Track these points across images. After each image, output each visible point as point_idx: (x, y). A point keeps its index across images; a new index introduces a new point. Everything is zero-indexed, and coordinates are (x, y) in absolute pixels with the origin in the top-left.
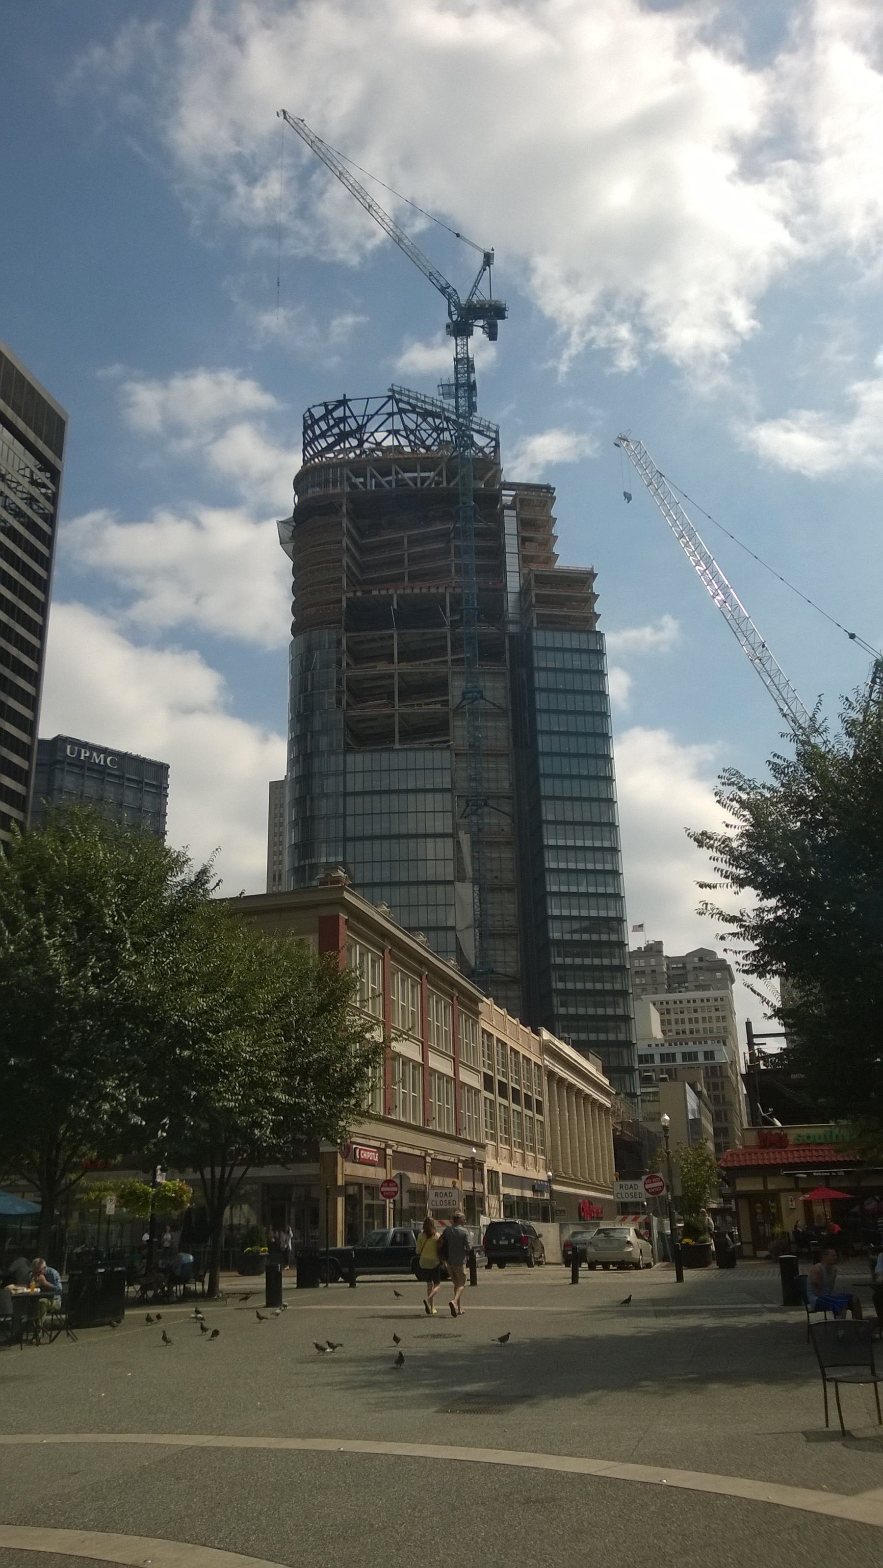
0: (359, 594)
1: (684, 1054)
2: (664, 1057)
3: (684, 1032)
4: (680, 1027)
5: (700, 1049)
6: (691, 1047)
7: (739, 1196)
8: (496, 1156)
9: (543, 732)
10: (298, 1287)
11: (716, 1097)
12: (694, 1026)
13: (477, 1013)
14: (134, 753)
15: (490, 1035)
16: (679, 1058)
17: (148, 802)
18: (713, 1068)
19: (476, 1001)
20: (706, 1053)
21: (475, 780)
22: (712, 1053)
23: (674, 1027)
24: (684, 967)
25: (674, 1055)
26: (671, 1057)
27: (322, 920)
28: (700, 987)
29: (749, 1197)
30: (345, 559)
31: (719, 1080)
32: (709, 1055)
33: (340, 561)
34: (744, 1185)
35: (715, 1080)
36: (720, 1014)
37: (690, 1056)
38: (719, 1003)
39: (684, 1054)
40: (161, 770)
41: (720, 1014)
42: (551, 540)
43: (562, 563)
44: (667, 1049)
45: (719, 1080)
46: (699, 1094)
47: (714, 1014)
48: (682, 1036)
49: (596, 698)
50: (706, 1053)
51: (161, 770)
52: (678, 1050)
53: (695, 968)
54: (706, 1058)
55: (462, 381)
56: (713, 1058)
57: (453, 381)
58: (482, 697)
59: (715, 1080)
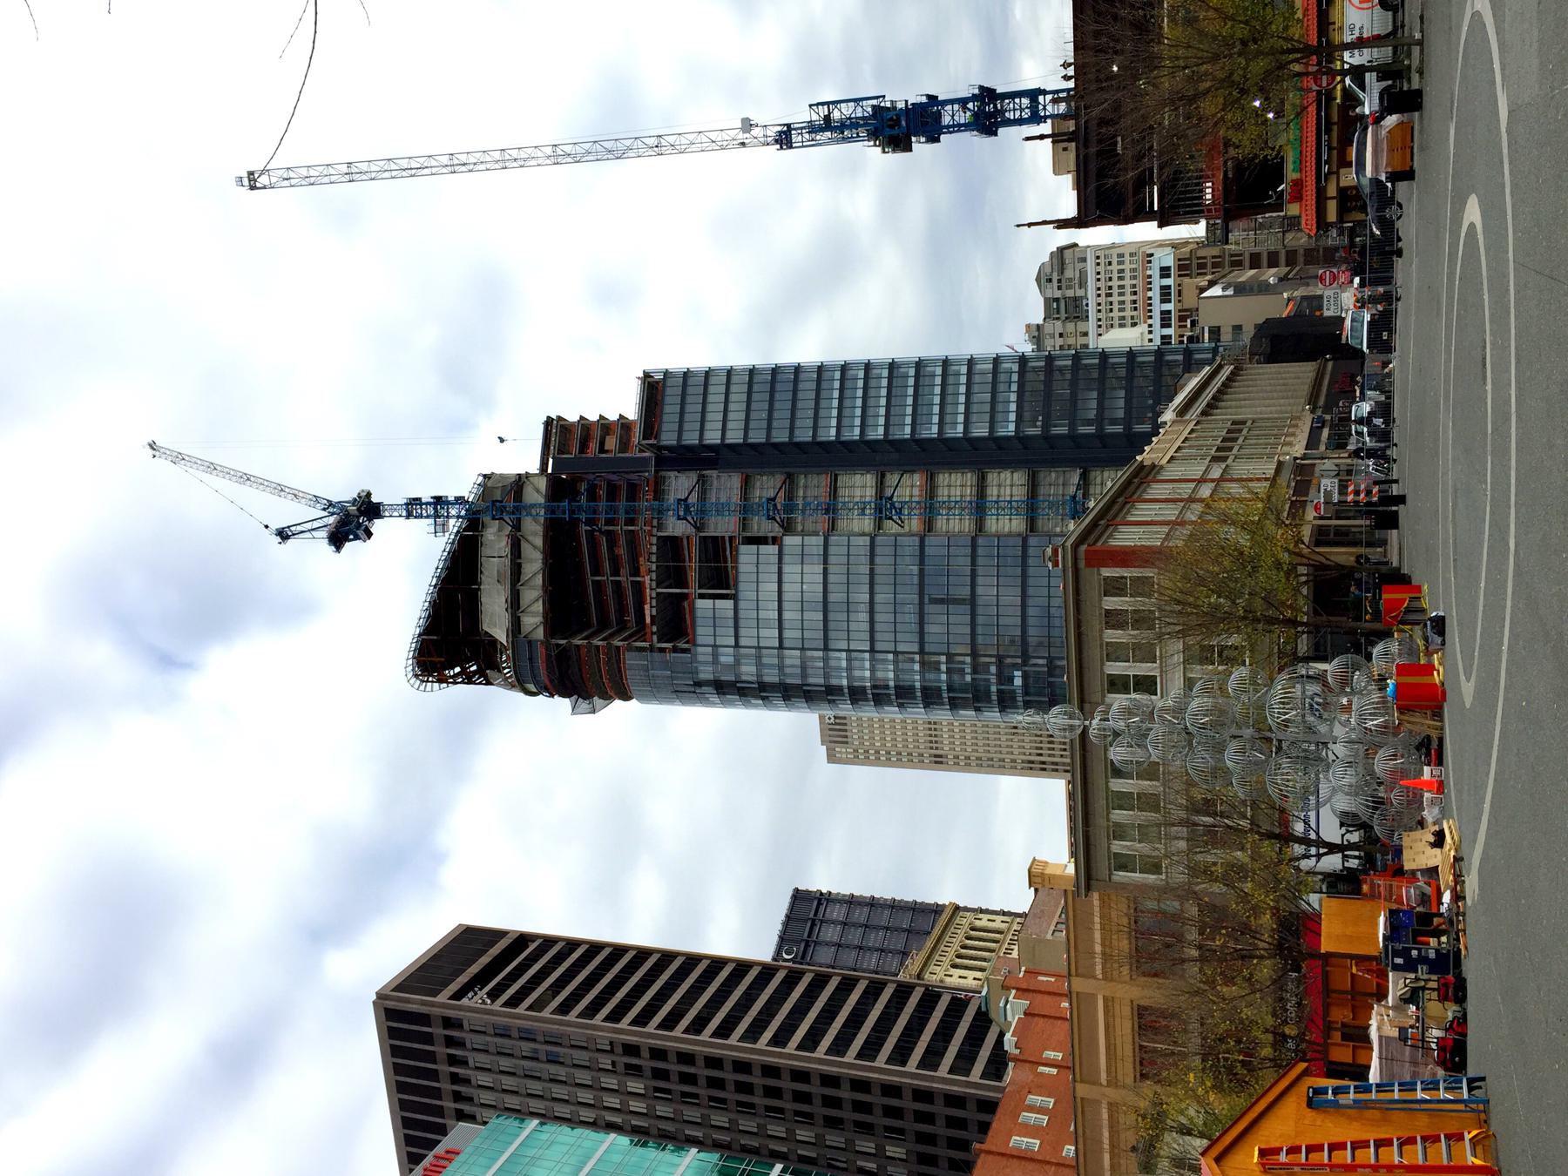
0: (654, 629)
1: (1163, 301)
2: (1165, 322)
3: (1135, 302)
4: (1128, 306)
5: (1157, 282)
6: (1155, 294)
7: (1341, 219)
8: (1290, 444)
9: (814, 435)
10: (1396, 527)
11: (1215, 265)
12: (1128, 290)
13: (1153, 466)
14: (780, 927)
15: (1172, 458)
16: (1167, 307)
17: (837, 913)
18: (1180, 267)
19: (1142, 466)
20: (1162, 276)
21: (863, 509)
22: (1162, 269)
23: (1128, 313)
24: (1057, 300)
25: (1162, 313)
26: (1165, 315)
27: (1089, 564)
28: (1083, 284)
29: (1342, 211)
30: (617, 643)
31: (1195, 262)
32: (1165, 272)
33: (618, 648)
34: (1332, 216)
35: (1194, 266)
36: (1115, 260)
37: (1165, 294)
38: (1101, 261)
39: (1163, 301)
40: (799, 897)
41: (1115, 260)
42: (604, 425)
43: (631, 411)
44: (1156, 321)
45: (1195, 262)
46: (1212, 284)
47: (1115, 267)
48: (1139, 305)
49: (779, 377)
50: (1162, 276)
51: (799, 897)
52: (1157, 307)
53: (1059, 288)
54: (1168, 276)
55: (431, 511)
56: (1168, 268)
57: (431, 521)
58: (774, 499)
59: (1194, 266)
